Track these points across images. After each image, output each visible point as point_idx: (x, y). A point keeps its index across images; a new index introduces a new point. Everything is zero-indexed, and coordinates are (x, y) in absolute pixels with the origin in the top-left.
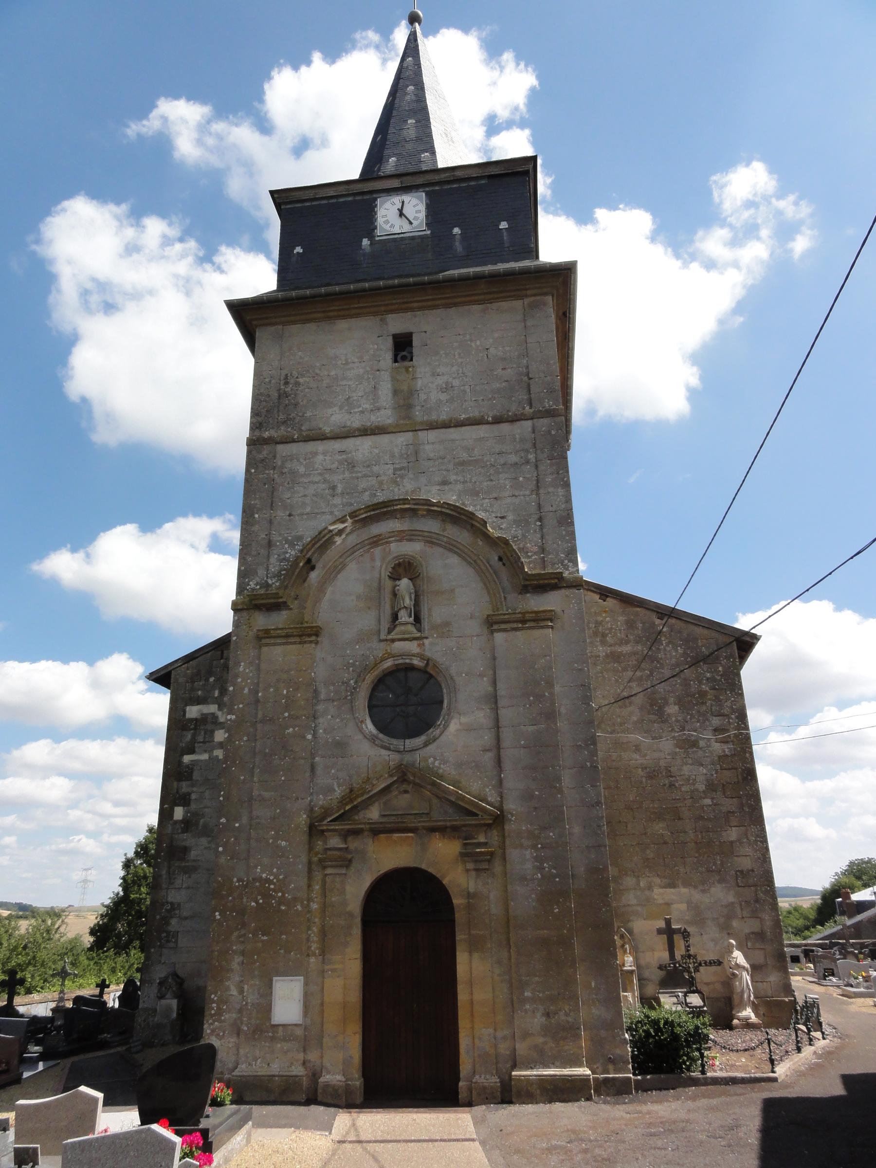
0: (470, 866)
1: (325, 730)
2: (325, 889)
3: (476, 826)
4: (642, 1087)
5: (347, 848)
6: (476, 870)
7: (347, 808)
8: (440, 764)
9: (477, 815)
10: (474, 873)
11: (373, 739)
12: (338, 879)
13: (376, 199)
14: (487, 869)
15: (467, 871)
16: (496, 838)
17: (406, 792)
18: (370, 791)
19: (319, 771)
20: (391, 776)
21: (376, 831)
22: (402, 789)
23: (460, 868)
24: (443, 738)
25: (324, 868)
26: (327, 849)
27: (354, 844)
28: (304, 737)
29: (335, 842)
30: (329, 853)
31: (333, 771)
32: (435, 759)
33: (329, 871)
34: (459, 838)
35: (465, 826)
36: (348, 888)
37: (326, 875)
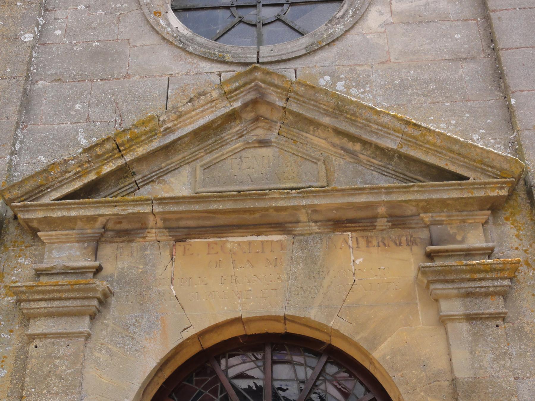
0: (453, 307)
1: (66, 32)
2: (22, 379)
3: (464, 205)
4: (220, 381)
5: (98, 270)
6: (470, 318)
7: (106, 169)
8: (347, 87)
9: (467, 178)
10: (464, 327)
11: (181, 46)
12: (63, 349)
13: (245, 389)
14: (502, 317)
15: (443, 321)
16: (516, 242)
17: (263, 143)
18: (169, 131)
19: (42, 108)
20: (227, 96)
21: (188, 227)
22: (252, 137)
23: (423, 319)
24: (353, 38)
25: (27, 319)
26: (39, 273)
27: (117, 261)
28: (16, 38)
29: (66, 253)
30: (44, 280)
31: (78, 106)
32: (336, 78)
33: (39, 327)
34: (411, 243)
35: (427, 206)
36: (91, 373)
37: (32, 338)
